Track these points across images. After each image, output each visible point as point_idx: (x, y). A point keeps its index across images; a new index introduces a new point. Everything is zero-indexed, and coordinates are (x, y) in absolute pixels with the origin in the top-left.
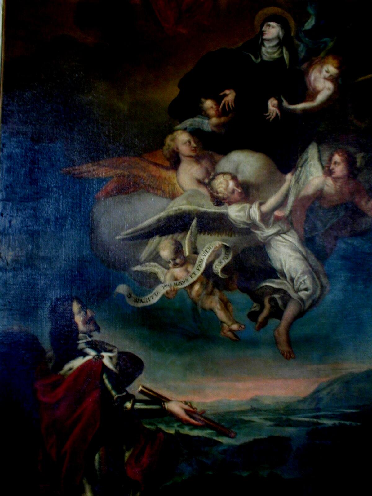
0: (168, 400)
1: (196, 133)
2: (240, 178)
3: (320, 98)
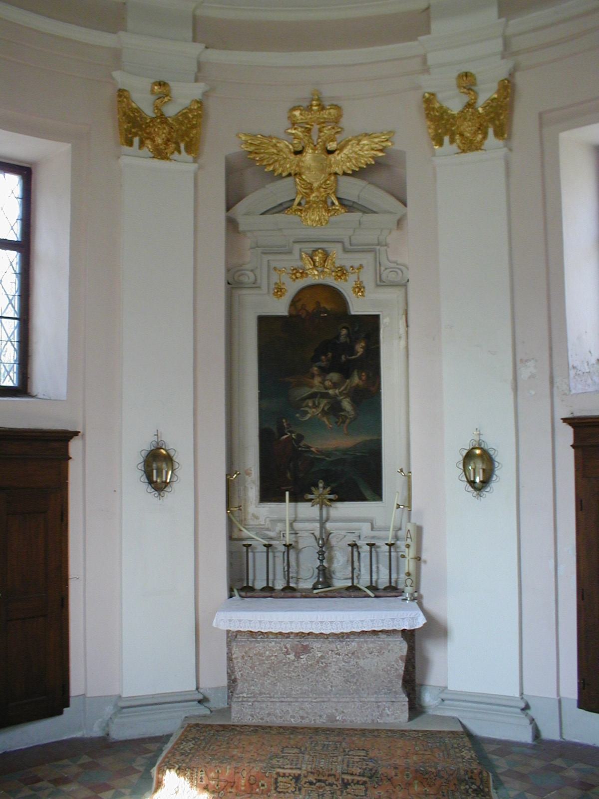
0: (311, 447)
1: (319, 367)
2: (333, 381)
3: (359, 354)
